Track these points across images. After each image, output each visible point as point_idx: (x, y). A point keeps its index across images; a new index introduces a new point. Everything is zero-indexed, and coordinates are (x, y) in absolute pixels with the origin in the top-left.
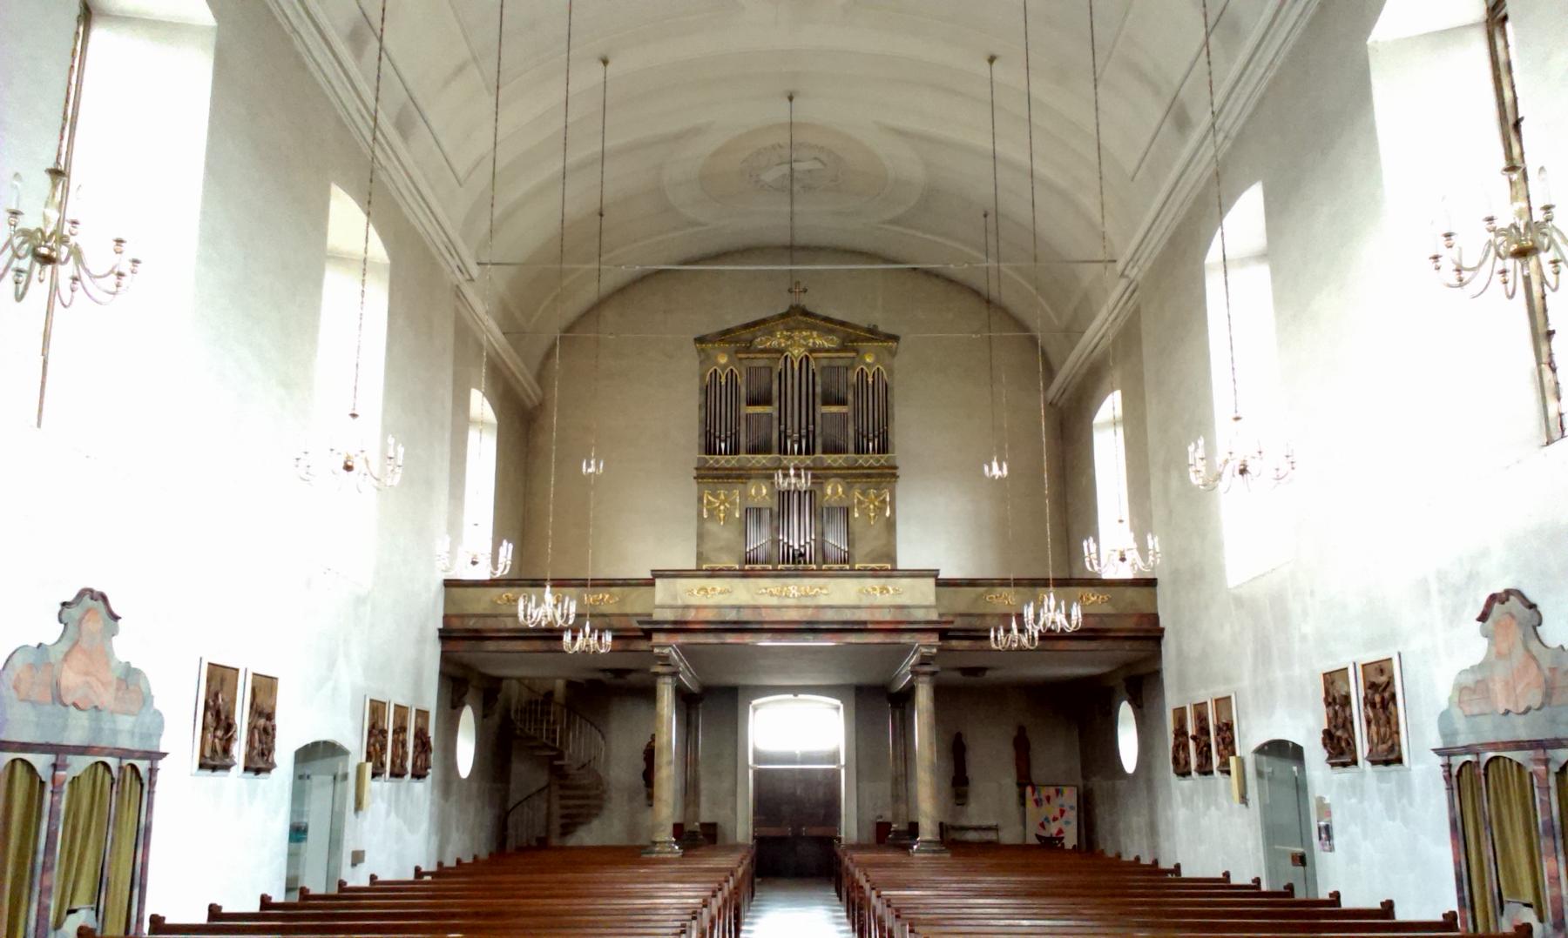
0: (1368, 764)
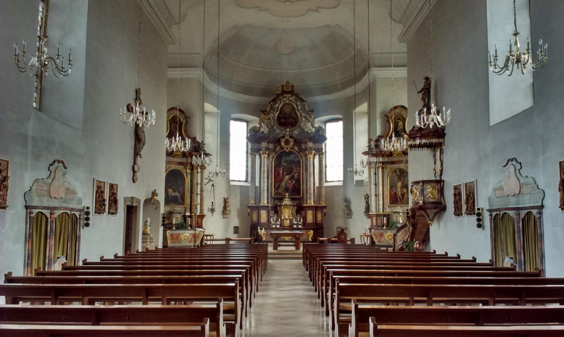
0: (465, 215)
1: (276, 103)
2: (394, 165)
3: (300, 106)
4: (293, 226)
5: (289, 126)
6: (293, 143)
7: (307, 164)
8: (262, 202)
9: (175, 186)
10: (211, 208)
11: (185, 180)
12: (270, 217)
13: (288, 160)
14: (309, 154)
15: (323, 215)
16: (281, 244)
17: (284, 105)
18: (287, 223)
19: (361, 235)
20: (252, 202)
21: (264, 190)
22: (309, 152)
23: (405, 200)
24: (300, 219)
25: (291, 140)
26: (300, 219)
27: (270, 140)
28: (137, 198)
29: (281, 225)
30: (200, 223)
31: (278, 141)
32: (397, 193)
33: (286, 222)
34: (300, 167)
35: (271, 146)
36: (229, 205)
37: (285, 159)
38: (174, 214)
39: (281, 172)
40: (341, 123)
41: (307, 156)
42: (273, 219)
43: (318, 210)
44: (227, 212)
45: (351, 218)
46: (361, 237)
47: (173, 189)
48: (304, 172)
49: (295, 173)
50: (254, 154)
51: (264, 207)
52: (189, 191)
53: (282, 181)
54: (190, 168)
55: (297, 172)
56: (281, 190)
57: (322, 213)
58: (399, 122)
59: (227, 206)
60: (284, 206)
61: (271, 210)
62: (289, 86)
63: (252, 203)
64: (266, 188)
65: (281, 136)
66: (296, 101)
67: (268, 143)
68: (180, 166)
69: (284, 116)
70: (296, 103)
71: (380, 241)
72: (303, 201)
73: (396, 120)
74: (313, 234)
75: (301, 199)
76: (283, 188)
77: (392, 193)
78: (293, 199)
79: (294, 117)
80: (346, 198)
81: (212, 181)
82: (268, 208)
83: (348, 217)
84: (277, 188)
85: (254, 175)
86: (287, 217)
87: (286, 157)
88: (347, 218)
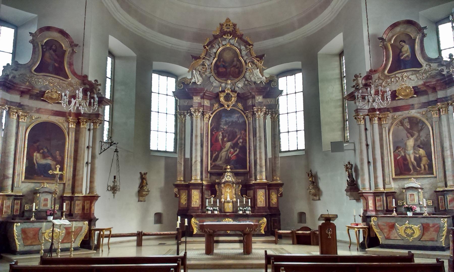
1: (212, 47)
2: (399, 113)
3: (244, 51)
4: (237, 211)
5: (231, 77)
6: (236, 99)
7: (256, 125)
8: (193, 178)
9: (47, 150)
10: (112, 186)
11: (65, 139)
12: (205, 199)
13: (229, 122)
14: (257, 111)
15: (279, 196)
16: (221, 238)
17: (223, 50)
18: (229, 208)
19: (348, 227)
20: (180, 179)
21: (196, 161)
22: (258, 109)
23: (423, 167)
24: (247, 202)
25: (234, 95)
26: (247, 202)
27: (204, 94)
28: (335, 225)
29: (220, 211)
30: (87, 209)
31: (217, 96)
32: (408, 157)
33: (228, 206)
34: (245, 131)
35: (207, 103)
36: (147, 184)
37: (226, 121)
38: (38, 195)
39: (220, 137)
40: (299, 76)
41: (255, 114)
42: (210, 202)
43: (272, 189)
44: (144, 193)
45: (319, 199)
46: (348, 230)
47: (43, 153)
48: (252, 137)
49: (239, 139)
50: (184, 113)
51: (196, 186)
52: (70, 158)
53: (221, 149)
54: (74, 122)
55: (241, 137)
56: (221, 162)
57: (277, 194)
58: (403, 46)
59: (144, 184)
60: (224, 183)
61: (206, 190)
62: (229, 25)
63: (181, 181)
64: (199, 159)
65: (220, 90)
66: (239, 45)
67: (202, 98)
68: (57, 118)
69: (223, 64)
70: (239, 48)
71: (388, 238)
72: (251, 177)
73: (398, 44)
74: (266, 223)
75: (247, 174)
76: (223, 158)
77: (398, 158)
78: (236, 174)
79: (236, 65)
80: (311, 171)
81: (115, 144)
82: (202, 187)
83: (315, 197)
84: (214, 160)
85: (183, 141)
86: (229, 199)
87: (227, 117)
88: (314, 200)
